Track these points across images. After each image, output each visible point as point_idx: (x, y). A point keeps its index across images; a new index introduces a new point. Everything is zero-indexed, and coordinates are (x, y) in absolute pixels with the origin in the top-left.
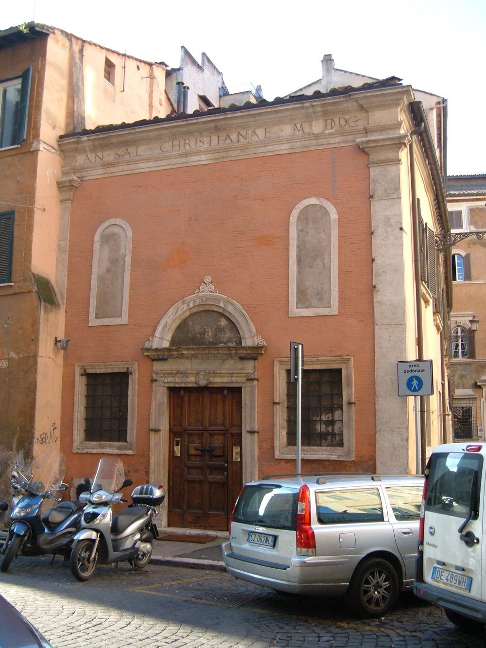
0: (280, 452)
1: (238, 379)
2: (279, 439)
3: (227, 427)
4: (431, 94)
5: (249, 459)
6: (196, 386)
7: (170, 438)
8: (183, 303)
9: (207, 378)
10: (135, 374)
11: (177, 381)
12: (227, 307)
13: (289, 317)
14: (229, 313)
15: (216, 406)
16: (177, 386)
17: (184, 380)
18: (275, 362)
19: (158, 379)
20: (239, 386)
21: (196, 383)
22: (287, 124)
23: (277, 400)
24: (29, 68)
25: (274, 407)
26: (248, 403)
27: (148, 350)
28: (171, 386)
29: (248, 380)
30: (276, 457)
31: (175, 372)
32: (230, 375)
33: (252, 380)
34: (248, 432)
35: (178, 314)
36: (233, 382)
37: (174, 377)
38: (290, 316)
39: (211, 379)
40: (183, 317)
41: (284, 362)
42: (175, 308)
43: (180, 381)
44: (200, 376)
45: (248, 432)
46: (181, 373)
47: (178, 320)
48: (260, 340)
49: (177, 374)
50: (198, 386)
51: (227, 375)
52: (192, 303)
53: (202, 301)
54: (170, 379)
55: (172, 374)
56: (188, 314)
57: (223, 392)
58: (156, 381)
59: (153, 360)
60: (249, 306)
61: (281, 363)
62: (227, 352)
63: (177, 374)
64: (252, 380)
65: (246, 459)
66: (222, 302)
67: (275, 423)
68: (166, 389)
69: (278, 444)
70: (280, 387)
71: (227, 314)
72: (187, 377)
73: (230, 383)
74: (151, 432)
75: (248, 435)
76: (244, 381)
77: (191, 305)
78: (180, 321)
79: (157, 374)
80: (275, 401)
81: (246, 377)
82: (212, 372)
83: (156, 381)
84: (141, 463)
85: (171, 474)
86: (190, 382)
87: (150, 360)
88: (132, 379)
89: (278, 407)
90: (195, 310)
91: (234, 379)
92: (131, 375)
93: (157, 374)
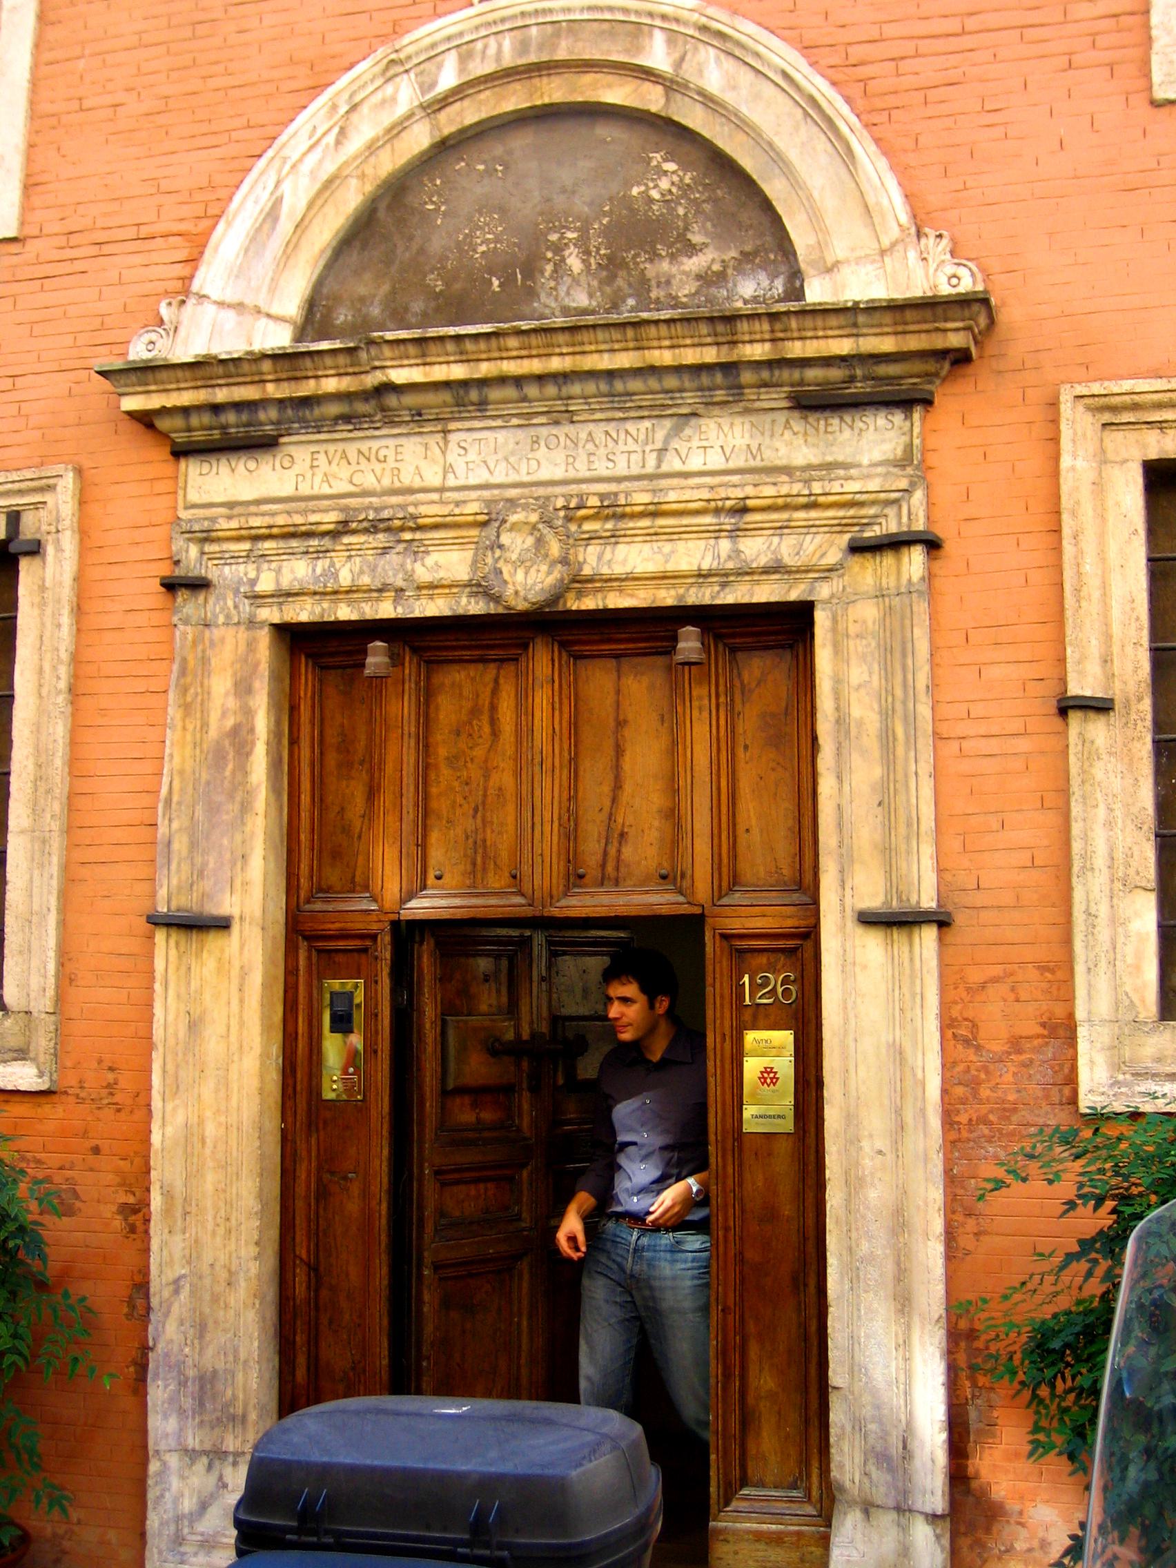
0: (1117, 1065)
1: (787, 549)
2: (1113, 963)
3: (703, 890)
4: (1042, 25)
5: (875, 1124)
6: (476, 607)
7: (291, 972)
8: (393, 68)
9: (555, 549)
10: (59, 549)
11: (345, 579)
12: (700, 72)
13: (1156, 104)
14: (708, 101)
15: (619, 751)
16: (345, 613)
17: (392, 568)
18: (1066, 408)
19: (211, 572)
20: (793, 596)
21: (478, 588)
22: (283, 1120)
23: (1082, 685)
24: (131, 414)
25: (1064, 734)
26: (863, 710)
27: (147, 372)
28: (304, 617)
29: (857, 549)
30: (1086, 1102)
31: (333, 516)
32: (728, 522)
33: (896, 544)
34: (868, 920)
35: (356, 143)
36: (745, 572)
37: (322, 552)
38: (1160, 94)
39: (592, 559)
40: (387, 164)
41: (1135, 407)
42: (334, 107)
43: (366, 580)
44: (505, 539)
45: (868, 920)
46: (373, 528)
47: (353, 182)
48: (950, 270)
49: (342, 529)
50: (493, 609)
51: (708, 519)
52: (451, 61)
53: (523, 46)
54: (298, 571)
55: (309, 535)
56: (420, 138)
57: (668, 646)
58: (199, 585)
59: (180, 452)
60: (857, 53)
61: (1107, 417)
62: (710, 355)
63: (342, 529)
64: (896, 544)
65: (850, 1118)
66: (659, 38)
67: (1077, 846)
68: (264, 638)
69: (1103, 1007)
70: (1105, 586)
71: (694, 117)
72: (415, 551)
73: (724, 577)
74: (160, 935)
75: (872, 945)
76: (833, 557)
77: (448, 79)
78: (369, 188)
79: (207, 537)
80: (1074, 689)
81: (843, 526)
82: (594, 501)
83: (199, 585)
84: (96, 1150)
85: (300, 1221)
86: (432, 586)
87: (165, 453)
88: (43, 588)
89: (1098, 730)
90: (469, 113)
91: (756, 549)
92: (36, 561)
93: (207, 537)
